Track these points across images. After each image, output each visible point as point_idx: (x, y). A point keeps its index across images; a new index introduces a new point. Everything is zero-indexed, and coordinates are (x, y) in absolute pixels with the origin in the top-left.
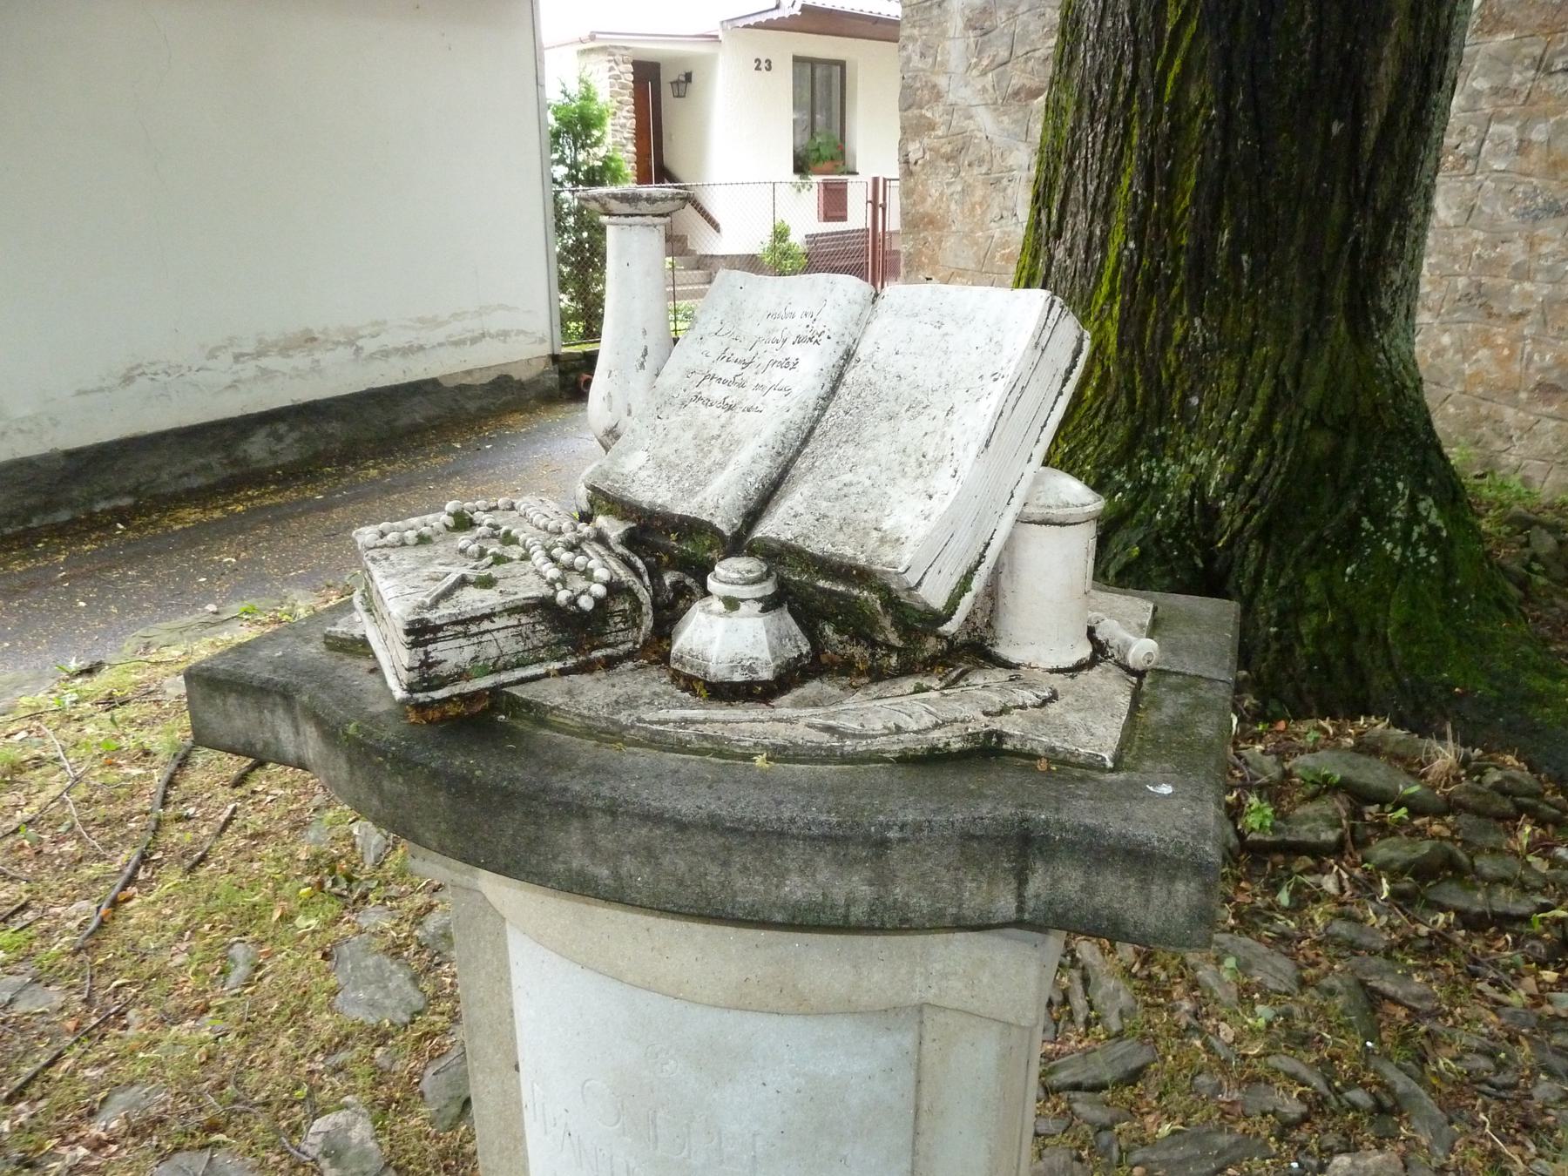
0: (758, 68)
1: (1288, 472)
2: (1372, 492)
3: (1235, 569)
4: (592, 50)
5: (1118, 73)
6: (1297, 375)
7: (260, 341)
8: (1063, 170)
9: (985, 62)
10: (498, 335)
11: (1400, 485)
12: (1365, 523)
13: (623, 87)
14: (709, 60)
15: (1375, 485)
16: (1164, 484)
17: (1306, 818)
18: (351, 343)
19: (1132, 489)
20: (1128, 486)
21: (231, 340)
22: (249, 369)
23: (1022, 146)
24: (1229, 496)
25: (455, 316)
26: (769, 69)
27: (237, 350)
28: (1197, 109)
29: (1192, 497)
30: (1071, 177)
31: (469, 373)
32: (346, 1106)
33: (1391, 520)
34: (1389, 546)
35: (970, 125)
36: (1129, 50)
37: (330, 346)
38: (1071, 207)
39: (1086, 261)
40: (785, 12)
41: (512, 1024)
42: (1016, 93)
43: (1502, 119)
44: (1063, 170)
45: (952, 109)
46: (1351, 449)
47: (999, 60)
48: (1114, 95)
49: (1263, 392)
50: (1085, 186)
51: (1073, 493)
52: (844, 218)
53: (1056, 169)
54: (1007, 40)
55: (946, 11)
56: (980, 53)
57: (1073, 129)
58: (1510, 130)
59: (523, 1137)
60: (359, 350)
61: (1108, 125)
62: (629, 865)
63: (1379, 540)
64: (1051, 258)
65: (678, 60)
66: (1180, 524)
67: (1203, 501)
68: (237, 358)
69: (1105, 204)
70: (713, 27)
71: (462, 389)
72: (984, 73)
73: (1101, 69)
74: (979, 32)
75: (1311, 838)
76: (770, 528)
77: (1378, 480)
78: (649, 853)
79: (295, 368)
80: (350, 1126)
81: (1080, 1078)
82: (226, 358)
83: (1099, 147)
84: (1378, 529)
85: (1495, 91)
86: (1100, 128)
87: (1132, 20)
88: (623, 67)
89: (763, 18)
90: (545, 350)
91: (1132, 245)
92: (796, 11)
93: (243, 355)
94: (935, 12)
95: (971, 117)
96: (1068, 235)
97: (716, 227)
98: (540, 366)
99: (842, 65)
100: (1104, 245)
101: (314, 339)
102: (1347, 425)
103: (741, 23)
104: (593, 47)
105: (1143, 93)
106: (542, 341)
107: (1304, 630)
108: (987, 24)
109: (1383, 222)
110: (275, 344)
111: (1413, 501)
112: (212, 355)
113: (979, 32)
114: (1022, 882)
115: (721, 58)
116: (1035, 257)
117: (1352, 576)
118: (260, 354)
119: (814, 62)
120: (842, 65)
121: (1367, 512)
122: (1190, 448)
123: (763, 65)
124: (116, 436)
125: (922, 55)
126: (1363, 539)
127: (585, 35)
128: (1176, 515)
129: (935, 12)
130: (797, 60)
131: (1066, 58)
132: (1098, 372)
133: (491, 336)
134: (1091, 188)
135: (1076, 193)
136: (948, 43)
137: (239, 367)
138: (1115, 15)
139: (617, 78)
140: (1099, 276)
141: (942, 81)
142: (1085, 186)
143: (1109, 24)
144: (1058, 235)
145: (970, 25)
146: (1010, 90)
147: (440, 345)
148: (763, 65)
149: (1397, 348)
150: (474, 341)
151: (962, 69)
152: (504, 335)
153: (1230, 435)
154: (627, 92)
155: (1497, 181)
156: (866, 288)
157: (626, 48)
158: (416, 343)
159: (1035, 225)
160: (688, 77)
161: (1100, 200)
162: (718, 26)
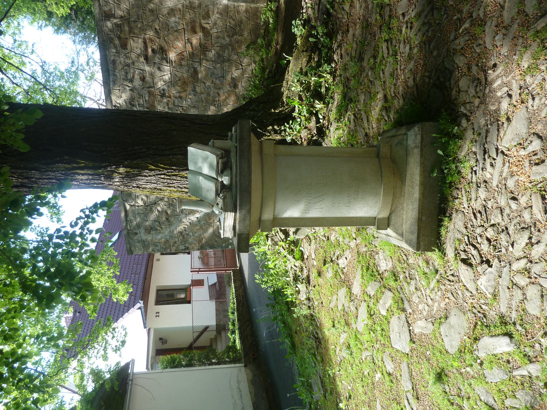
5: (163, 178)
9: (159, 228)
10: (239, 384)
14: (156, 330)
26: (159, 313)
31: (250, 393)
45: (171, 237)
47: (158, 224)
48: (168, 179)
52: (203, 280)
55: (146, 240)
65: (155, 342)
70: (145, 331)
71: (256, 395)
72: (162, 228)
76: (215, 176)
90: (243, 369)
94: (146, 243)
98: (248, 371)
106: (240, 370)
123: (158, 314)
125: (157, 246)
129: (146, 243)
133: (239, 386)
145: (149, 233)
147: (242, 402)
148: (158, 314)
150: (240, 391)
152: (238, 382)
160: (161, 339)
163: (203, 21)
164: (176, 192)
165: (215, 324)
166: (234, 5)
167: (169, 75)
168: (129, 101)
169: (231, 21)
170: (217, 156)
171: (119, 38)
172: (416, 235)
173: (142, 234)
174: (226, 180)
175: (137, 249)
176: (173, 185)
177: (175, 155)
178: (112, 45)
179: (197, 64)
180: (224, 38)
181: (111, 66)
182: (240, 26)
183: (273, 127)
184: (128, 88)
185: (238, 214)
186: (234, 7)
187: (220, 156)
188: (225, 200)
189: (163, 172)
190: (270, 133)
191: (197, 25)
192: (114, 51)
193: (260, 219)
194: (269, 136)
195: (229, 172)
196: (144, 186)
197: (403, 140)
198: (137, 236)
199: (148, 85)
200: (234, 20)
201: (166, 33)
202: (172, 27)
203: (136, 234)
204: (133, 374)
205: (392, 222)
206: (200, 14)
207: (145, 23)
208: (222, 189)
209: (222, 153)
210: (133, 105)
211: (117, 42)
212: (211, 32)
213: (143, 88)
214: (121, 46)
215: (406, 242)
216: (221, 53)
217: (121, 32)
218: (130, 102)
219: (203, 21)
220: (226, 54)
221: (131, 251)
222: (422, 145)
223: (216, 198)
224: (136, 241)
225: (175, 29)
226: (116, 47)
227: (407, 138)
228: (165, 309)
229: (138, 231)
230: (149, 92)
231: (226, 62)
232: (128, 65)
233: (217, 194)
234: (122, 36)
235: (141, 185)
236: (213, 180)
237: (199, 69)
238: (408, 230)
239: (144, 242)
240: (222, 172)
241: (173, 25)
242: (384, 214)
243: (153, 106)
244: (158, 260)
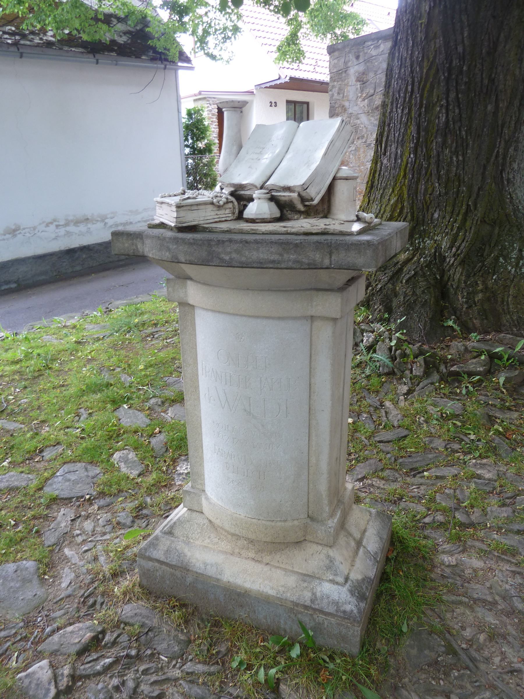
0: (271, 106)
1: (471, 241)
2: (504, 248)
3: (451, 279)
4: (200, 99)
6: (475, 205)
7: (66, 220)
8: (386, 129)
9: (364, 95)
11: (515, 245)
12: (501, 259)
13: (213, 115)
15: (506, 245)
16: (424, 248)
17: (473, 363)
18: (103, 221)
19: (412, 250)
20: (411, 249)
21: (55, 220)
22: (62, 231)
24: (449, 251)
25: (145, 210)
26: (276, 106)
27: (57, 223)
28: (436, 102)
29: (435, 252)
30: (389, 131)
32: (126, 449)
33: (511, 258)
34: (510, 268)
35: (358, 122)
36: (410, 80)
37: (94, 222)
38: (389, 143)
39: (395, 163)
40: (282, 81)
41: (196, 348)
44: (386, 129)
46: (496, 231)
47: (370, 94)
48: (405, 98)
49: (463, 211)
50: (394, 134)
53: (384, 129)
54: (373, 85)
55: (348, 75)
56: (362, 91)
57: (390, 112)
59: (198, 386)
60: (106, 224)
61: (403, 110)
62: (234, 255)
63: (506, 266)
64: (382, 164)
66: (430, 262)
67: (440, 254)
68: (57, 226)
69: (402, 140)
70: (251, 87)
73: (400, 88)
74: (361, 83)
75: (474, 369)
77: (506, 244)
78: (238, 252)
79: (80, 231)
80: (128, 454)
81: (382, 439)
82: (52, 227)
83: (399, 119)
84: (506, 261)
86: (400, 111)
87: (411, 68)
88: (213, 106)
89: (273, 84)
91: (412, 156)
92: (287, 79)
93: (59, 225)
94: (344, 75)
95: (358, 119)
96: (388, 154)
99: (308, 103)
100: (401, 157)
101: (88, 219)
102: (495, 223)
103: (264, 86)
104: (201, 97)
105: (416, 97)
107: (476, 299)
108: (365, 79)
109: (508, 144)
110: (72, 221)
112: (47, 225)
113: (361, 83)
114: (331, 257)
116: (376, 164)
117: (495, 279)
118: (67, 224)
119: (295, 103)
120: (308, 103)
121: (502, 255)
122: (435, 234)
123: (273, 104)
124: (10, 259)
125: (339, 93)
126: (499, 266)
127: (197, 92)
128: (429, 259)
130: (288, 102)
131: (388, 85)
132: (400, 206)
134: (397, 135)
135: (391, 137)
136: (349, 88)
137: (57, 231)
138: (405, 67)
139: (211, 111)
140: (400, 169)
141: (346, 104)
142: (394, 134)
143: (403, 70)
144: (385, 154)
145: (358, 80)
146: (374, 106)
148: (273, 104)
149: (516, 194)
151: (354, 99)
153: (449, 227)
154: (215, 117)
156: (296, 124)
157: (214, 98)
158: (129, 221)
159: (376, 152)
161: (400, 139)
162: (254, 88)
170: (305, 187)
172: (162, 558)
173: (356, 68)
175: (336, 61)
176: (394, 110)
183: (482, 291)
185: (169, 234)
187: (304, 194)
188: (210, 207)
189: (416, 89)
193: (191, 279)
194: (465, 282)
195: (277, 213)
196: (397, 55)
197: (336, 575)
198: (354, 60)
203: (358, 58)
204: (176, 71)
209: (312, 200)
221: (333, 52)
222: (315, 610)
224: (347, 59)
227: (337, 583)
229: (361, 60)
235: (399, 49)
236: (264, 179)
238: (173, 546)
239: (346, 72)
240: (272, 199)
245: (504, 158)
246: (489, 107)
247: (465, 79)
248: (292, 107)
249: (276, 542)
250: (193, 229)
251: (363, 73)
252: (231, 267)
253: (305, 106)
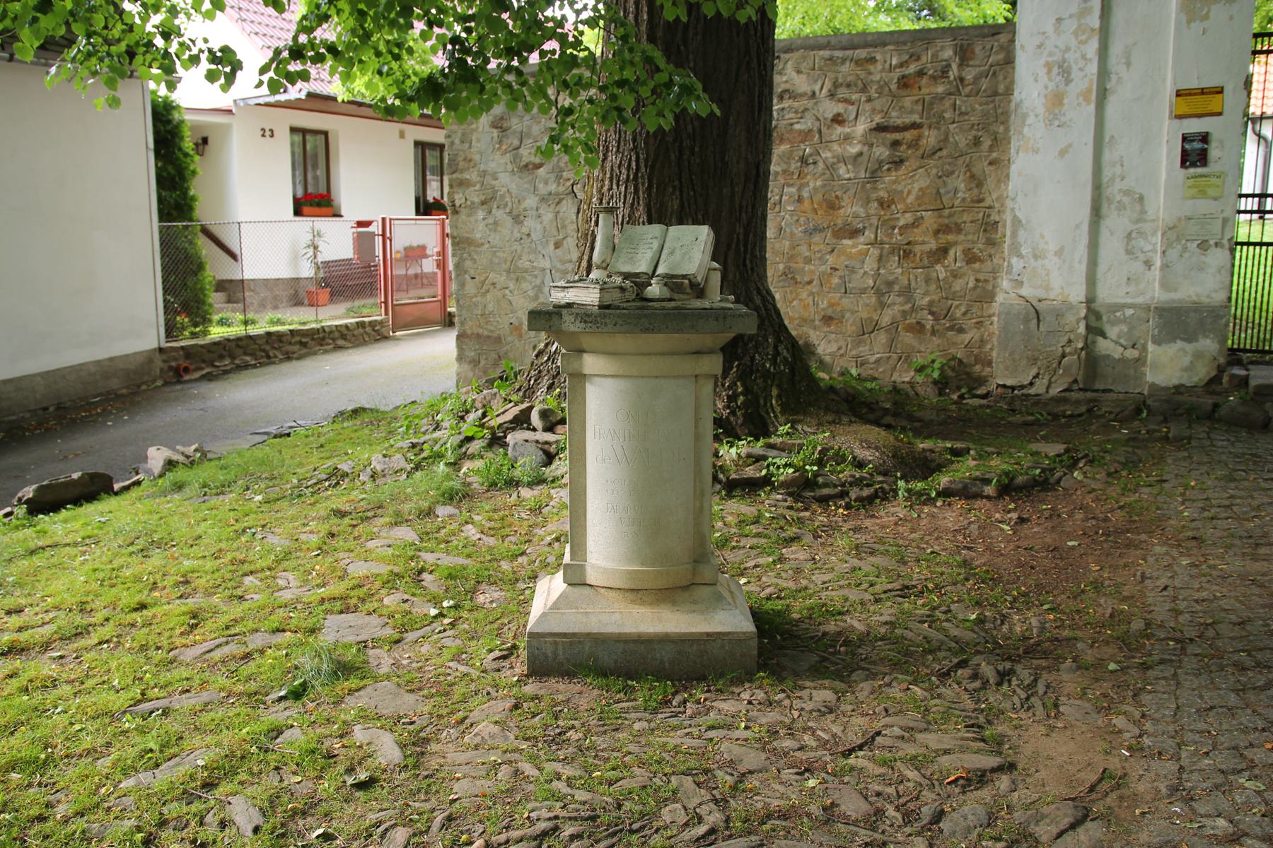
0: (263, 136)
14: (226, 129)
23: (532, 196)
26: (272, 136)
31: (111, 359)
42: (526, 166)
43: (790, 185)
45: (484, 174)
51: (716, 265)
58: (793, 190)
76: (660, 271)
85: (784, 172)
86: (623, 189)
97: (233, 256)
99: (326, 133)
103: (253, 102)
111: (776, 347)
115: (235, 128)
123: (268, 133)
125: (462, 142)
130: (294, 130)
148: (268, 133)
155: (791, 216)
163: (959, 249)
164: (599, 191)
165: (246, 277)
166: (993, 315)
167: (847, 176)
168: (791, 88)
169: (963, 309)
171: (921, 73)
174: (655, 290)
177: (681, 192)
178: (906, 57)
179: (873, 236)
180: (926, 294)
181: (862, 53)
182: (951, 328)
183: (742, 393)
184: (817, 88)
186: (990, 316)
189: (642, 165)
190: (730, 387)
191: (951, 238)
192: (894, 63)
199: (824, 130)
200: (964, 314)
201: (934, 171)
202: (945, 184)
205: (577, 590)
206: (974, 242)
207: (952, 127)
208: (639, 282)
210: (781, 98)
211: (912, 68)
212: (938, 267)
213: (818, 119)
214: (903, 77)
215: (544, 615)
216: (896, 288)
217: (934, 78)
218: (787, 91)
219: (959, 249)
220: (892, 298)
223: (621, 274)
225: (942, 191)
226: (901, 65)
228: (280, 155)
230: (810, 131)
231: (879, 298)
232: (864, 89)
233: (627, 276)
234: (925, 81)
237: (862, 239)
241: (950, 187)
242: (592, 578)
243: (782, 140)
244: (402, 135)
245: (745, 246)
246: (725, 191)
247: (698, 161)
248: (298, 138)
249: (637, 592)
250: (608, 307)
251: (502, 118)
252: (1096, 213)
253: (323, 137)
